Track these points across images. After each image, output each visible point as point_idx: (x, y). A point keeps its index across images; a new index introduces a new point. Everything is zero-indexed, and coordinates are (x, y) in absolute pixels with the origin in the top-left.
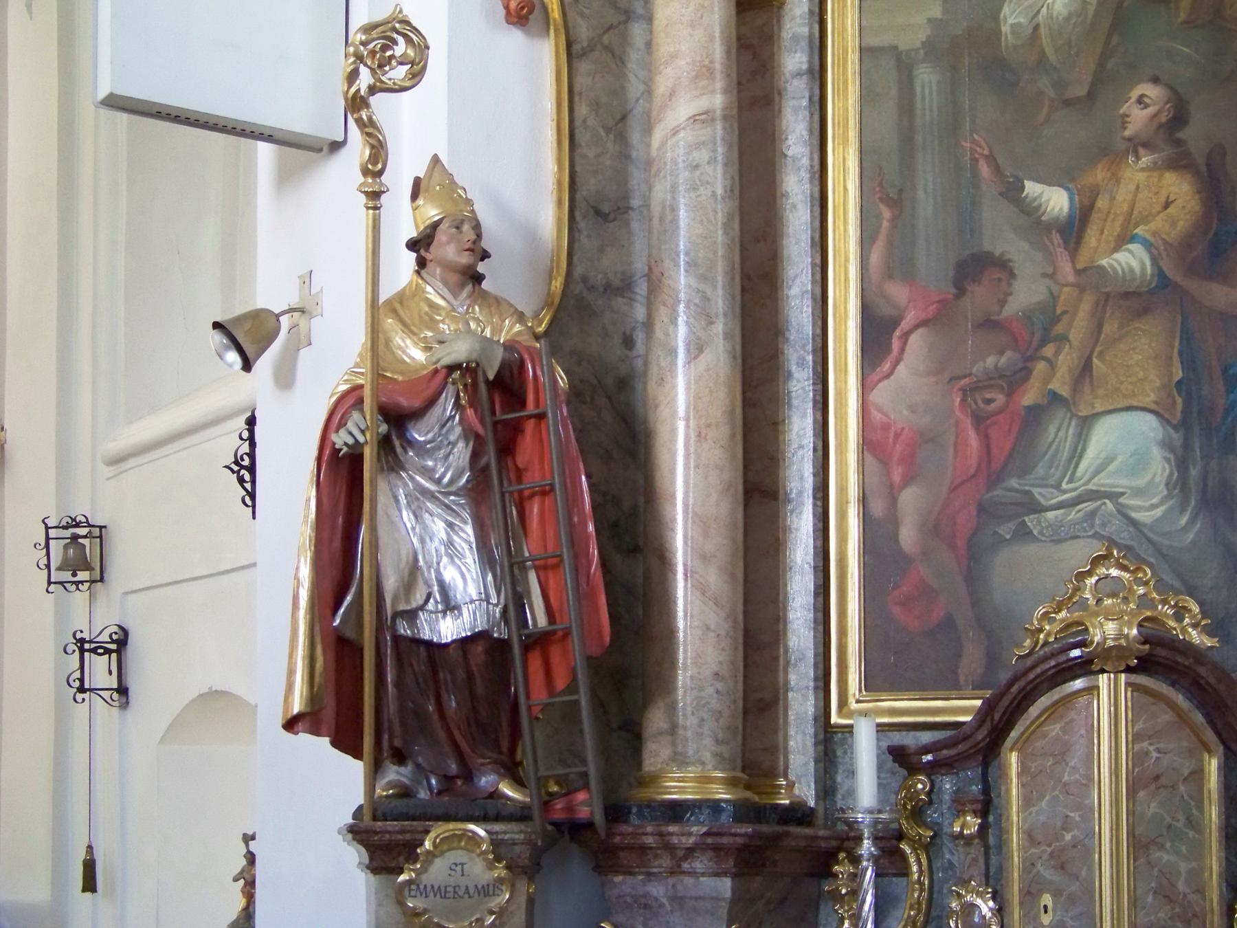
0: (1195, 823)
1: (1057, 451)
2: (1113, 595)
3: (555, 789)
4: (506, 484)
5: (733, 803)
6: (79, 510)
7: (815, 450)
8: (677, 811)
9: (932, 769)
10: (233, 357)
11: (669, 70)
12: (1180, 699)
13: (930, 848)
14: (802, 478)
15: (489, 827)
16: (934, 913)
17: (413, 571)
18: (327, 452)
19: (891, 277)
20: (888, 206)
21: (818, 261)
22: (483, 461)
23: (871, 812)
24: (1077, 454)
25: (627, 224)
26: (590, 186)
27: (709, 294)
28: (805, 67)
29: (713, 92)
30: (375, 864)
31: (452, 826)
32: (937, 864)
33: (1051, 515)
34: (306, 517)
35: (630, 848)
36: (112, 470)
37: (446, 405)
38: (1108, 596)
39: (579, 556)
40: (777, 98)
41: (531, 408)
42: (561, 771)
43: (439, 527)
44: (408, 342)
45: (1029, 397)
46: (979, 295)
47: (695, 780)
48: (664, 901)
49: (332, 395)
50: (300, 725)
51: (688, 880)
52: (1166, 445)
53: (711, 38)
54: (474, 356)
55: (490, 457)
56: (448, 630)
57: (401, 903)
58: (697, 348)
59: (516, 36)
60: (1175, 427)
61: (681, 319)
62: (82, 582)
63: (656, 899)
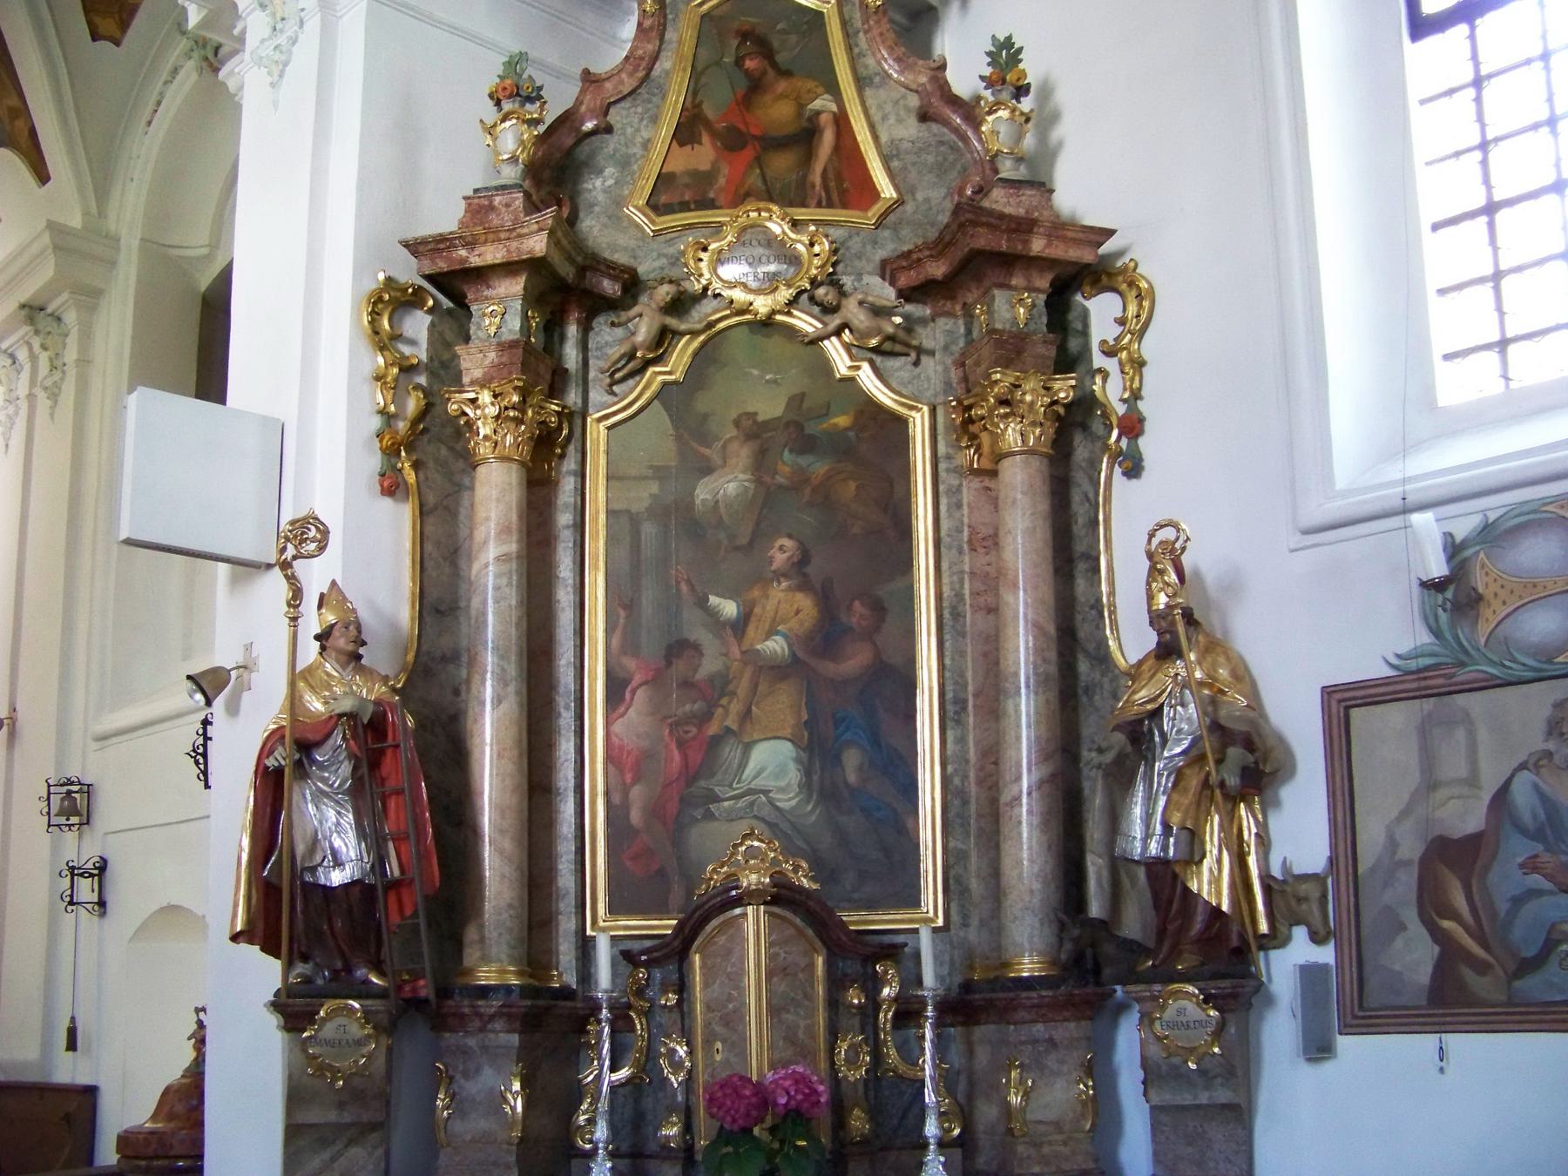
0: (809, 996)
1: (730, 764)
2: (755, 858)
3: (407, 977)
4: (374, 786)
5: (520, 986)
6: (73, 772)
7: (575, 762)
8: (485, 992)
9: (648, 965)
10: (199, 697)
11: (483, 528)
12: (798, 921)
13: (647, 1014)
14: (567, 780)
15: (362, 1002)
16: (651, 1055)
17: (314, 844)
18: (261, 768)
19: (625, 653)
20: (624, 609)
21: (578, 643)
22: (360, 773)
23: (606, 992)
24: (743, 765)
25: (457, 618)
26: (433, 594)
27: (506, 667)
28: (571, 522)
29: (511, 542)
30: (290, 1025)
31: (338, 1001)
32: (653, 1024)
33: (726, 804)
34: (247, 808)
35: (454, 1015)
36: (96, 745)
37: (337, 739)
38: (752, 858)
39: (420, 833)
40: (553, 541)
41: (390, 741)
42: (411, 966)
43: (331, 814)
44: (314, 698)
45: (713, 729)
46: (680, 667)
47: (495, 972)
48: (476, 1049)
49: (265, 731)
50: (241, 939)
51: (492, 1036)
52: (798, 760)
53: (511, 509)
54: (355, 709)
55: (364, 770)
56: (337, 878)
57: (305, 1051)
58: (498, 700)
59: (387, 502)
60: (804, 750)
61: (489, 683)
62: (73, 825)
63: (471, 1048)
